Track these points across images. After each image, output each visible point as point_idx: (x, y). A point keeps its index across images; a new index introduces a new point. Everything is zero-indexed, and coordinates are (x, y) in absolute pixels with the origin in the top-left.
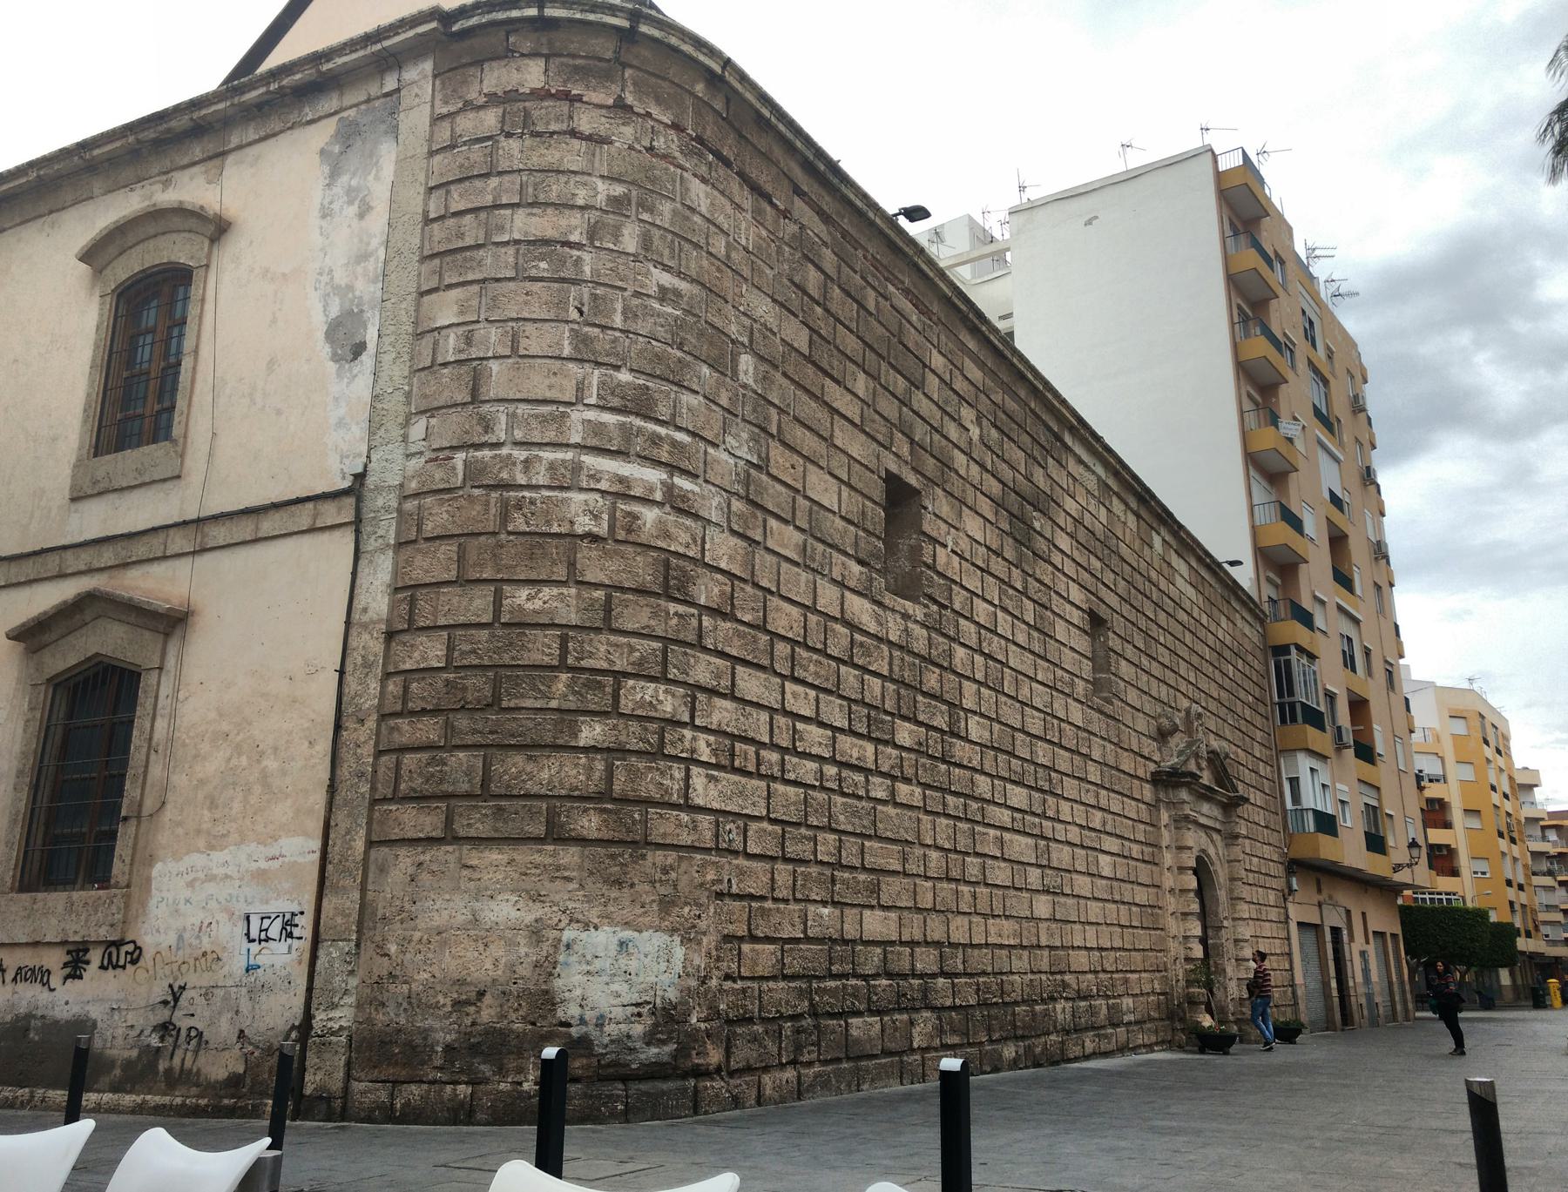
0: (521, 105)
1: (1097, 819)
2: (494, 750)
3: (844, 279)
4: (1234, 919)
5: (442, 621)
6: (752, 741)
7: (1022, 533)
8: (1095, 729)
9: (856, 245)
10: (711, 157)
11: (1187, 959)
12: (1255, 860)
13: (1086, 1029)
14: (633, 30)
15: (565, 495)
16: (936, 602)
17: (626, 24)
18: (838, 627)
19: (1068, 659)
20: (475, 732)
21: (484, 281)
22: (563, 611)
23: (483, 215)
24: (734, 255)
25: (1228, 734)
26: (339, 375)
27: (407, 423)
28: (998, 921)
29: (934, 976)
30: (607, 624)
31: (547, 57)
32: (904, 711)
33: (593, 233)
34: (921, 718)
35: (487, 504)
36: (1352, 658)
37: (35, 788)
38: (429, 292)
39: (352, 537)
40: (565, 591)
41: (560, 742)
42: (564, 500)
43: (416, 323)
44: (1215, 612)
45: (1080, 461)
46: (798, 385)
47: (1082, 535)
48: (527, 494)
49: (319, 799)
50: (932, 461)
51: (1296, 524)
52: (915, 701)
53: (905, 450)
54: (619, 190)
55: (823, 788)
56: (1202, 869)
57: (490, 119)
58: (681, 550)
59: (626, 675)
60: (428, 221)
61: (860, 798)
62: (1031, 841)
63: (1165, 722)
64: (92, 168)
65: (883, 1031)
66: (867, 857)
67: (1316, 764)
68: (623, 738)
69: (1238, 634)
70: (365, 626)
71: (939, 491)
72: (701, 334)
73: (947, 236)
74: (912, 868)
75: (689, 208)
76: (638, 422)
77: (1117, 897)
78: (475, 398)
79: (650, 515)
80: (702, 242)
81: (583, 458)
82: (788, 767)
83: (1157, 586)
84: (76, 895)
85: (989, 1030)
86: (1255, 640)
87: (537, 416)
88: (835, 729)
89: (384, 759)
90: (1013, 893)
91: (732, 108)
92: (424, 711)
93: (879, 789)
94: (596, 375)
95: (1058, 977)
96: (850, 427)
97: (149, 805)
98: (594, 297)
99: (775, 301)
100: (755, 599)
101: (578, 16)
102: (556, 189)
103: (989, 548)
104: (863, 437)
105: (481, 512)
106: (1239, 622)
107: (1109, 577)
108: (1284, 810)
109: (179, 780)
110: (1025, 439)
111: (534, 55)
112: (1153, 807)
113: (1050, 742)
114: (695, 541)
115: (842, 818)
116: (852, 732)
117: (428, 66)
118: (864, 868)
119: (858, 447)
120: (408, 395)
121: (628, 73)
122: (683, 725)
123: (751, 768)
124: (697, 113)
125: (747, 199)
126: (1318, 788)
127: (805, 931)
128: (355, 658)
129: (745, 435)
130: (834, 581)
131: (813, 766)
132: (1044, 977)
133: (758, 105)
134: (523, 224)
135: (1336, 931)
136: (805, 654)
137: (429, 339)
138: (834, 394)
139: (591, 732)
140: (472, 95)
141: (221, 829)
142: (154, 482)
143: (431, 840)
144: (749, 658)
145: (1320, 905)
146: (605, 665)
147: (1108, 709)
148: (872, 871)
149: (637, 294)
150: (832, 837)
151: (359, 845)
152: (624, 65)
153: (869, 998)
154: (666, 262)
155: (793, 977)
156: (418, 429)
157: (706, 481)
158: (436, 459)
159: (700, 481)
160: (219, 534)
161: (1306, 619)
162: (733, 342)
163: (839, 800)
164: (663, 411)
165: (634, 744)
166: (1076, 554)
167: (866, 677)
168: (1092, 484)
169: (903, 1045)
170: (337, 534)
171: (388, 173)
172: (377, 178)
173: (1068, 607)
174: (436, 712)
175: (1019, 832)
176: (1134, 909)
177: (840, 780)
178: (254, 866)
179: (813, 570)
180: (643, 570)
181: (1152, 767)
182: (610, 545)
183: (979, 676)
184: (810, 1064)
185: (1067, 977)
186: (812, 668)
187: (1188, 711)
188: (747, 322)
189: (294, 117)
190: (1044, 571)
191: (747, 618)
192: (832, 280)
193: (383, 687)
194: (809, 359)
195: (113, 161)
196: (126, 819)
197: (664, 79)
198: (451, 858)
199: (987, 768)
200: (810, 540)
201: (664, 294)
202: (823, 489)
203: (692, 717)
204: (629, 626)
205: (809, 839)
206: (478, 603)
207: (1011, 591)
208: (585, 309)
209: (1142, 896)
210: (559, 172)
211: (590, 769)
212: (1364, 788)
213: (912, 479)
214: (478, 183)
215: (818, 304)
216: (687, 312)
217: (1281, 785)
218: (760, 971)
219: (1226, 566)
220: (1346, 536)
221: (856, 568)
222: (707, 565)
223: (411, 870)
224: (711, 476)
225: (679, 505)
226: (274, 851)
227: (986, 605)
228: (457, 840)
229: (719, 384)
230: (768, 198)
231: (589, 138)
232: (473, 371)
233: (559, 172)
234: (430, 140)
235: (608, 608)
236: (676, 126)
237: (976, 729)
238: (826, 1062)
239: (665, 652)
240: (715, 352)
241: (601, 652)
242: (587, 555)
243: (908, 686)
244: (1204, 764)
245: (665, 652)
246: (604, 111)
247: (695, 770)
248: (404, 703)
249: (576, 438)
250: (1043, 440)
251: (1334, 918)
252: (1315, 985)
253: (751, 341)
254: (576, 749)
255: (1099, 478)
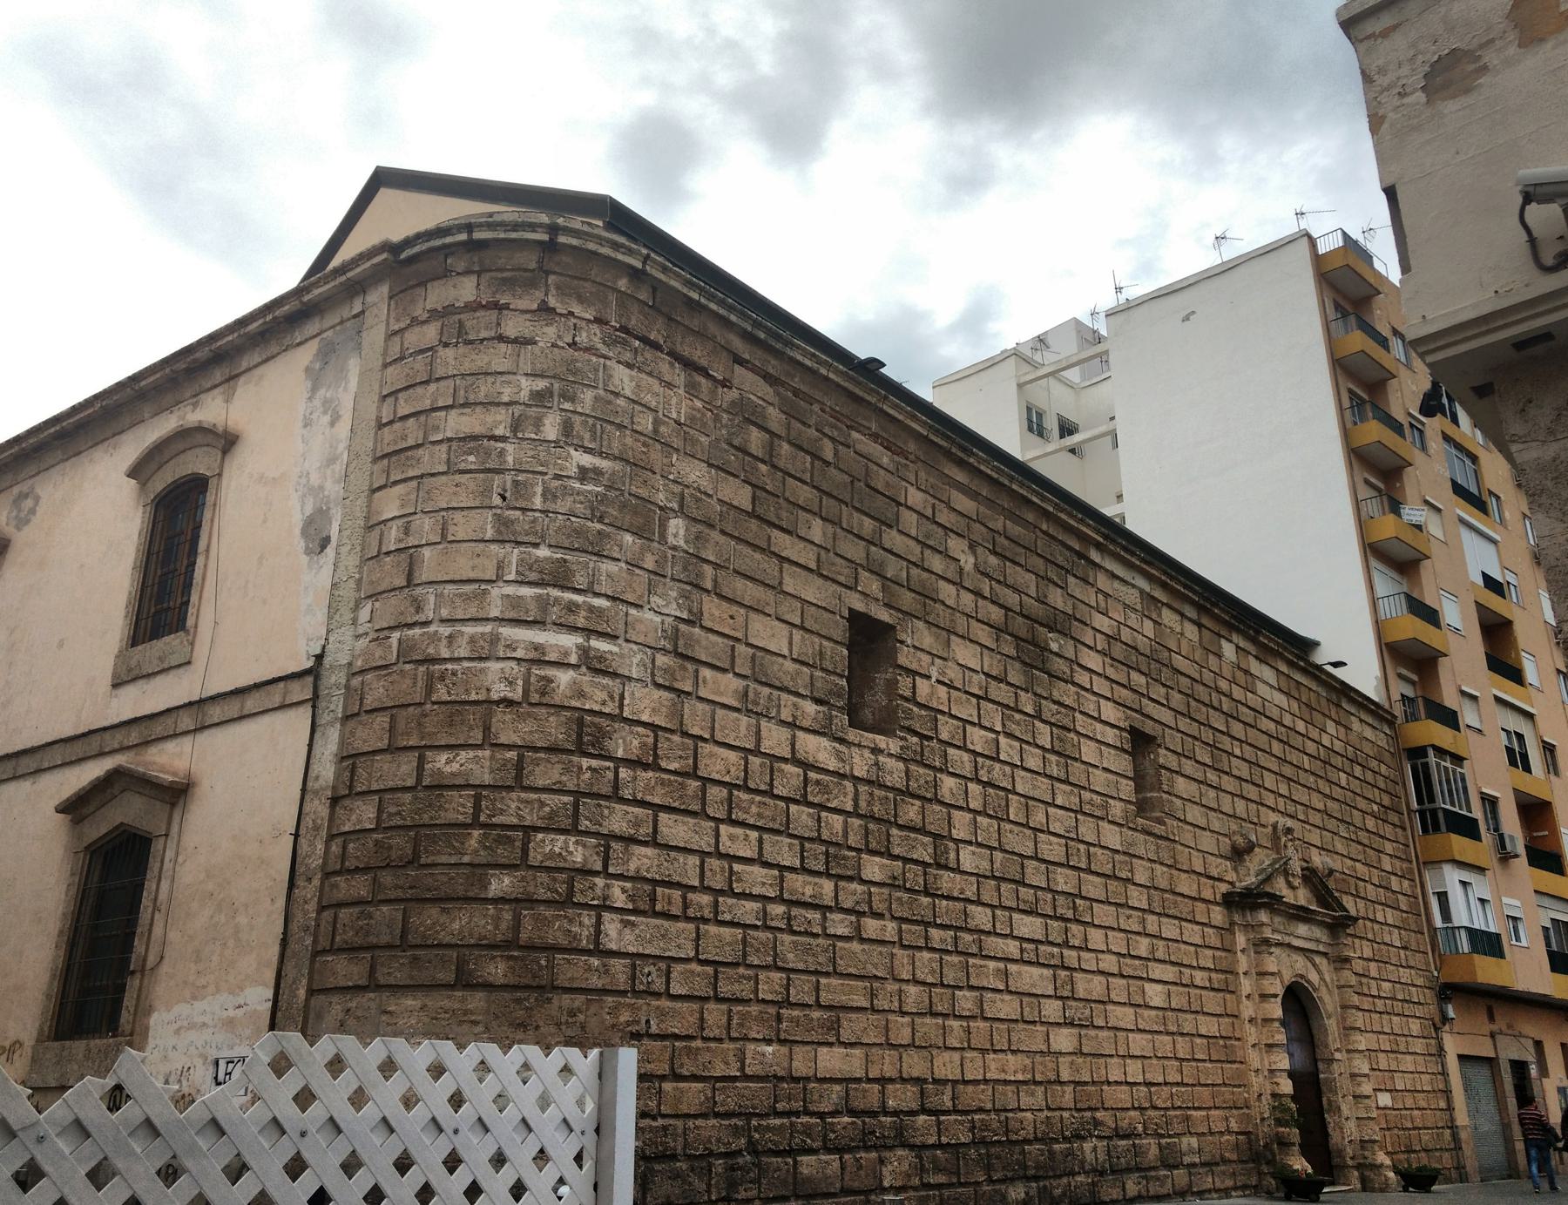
1: (1142, 946)
2: (412, 904)
3: (793, 434)
4: (1349, 1051)
5: (375, 787)
6: (678, 885)
7: (1033, 657)
8: (1141, 851)
9: (811, 400)
10: (637, 343)
11: (1274, 1095)
12: (1386, 985)
13: (1129, 1170)
16: (916, 733)
17: (546, 237)
19: (1099, 780)
20: (397, 887)
21: (422, 476)
23: (422, 418)
24: (663, 429)
25: (1339, 847)
26: (310, 567)
27: (356, 608)
28: (1001, 1056)
29: (912, 1113)
30: (519, 784)
31: (479, 273)
32: (873, 845)
33: (516, 426)
34: (896, 851)
35: (415, 678)
36: (1524, 757)
38: (380, 488)
39: (310, 710)
40: (480, 753)
41: (471, 894)
42: (482, 670)
43: (367, 518)
44: (1318, 717)
45: (1114, 576)
46: (739, 540)
47: (1118, 650)
48: (449, 666)
50: (910, 595)
51: (1431, 616)
52: (889, 835)
54: (541, 384)
56: (1298, 1001)
57: (430, 333)
58: (596, 708)
59: (536, 829)
60: (381, 426)
61: (816, 936)
62: (1047, 972)
63: (1240, 840)
64: (142, 396)
65: (843, 1169)
66: (823, 994)
67: (1466, 876)
68: (531, 889)
69: (1353, 738)
70: (316, 793)
71: (920, 624)
72: (623, 506)
73: (1050, 341)
75: (612, 392)
77: (1173, 1029)
78: (410, 583)
79: (564, 678)
80: (626, 422)
81: (501, 630)
82: (721, 908)
83: (1230, 696)
85: (988, 1168)
86: (1383, 744)
87: (460, 595)
88: (782, 868)
89: (325, 914)
90: (1021, 1026)
91: (659, 295)
93: (840, 925)
95: (1088, 1114)
96: (804, 573)
97: (152, 959)
98: (516, 483)
99: (710, 465)
100: (684, 747)
101: (502, 235)
102: (484, 389)
103: (987, 675)
104: (820, 581)
105: (408, 685)
106: (1356, 726)
107: (1158, 692)
108: (1433, 931)
109: (173, 935)
110: (1039, 563)
111: (468, 272)
112: (1230, 929)
113: (1073, 868)
114: (612, 697)
115: (790, 956)
117: (384, 289)
118: (819, 1006)
119: (813, 590)
120: (359, 582)
121: (551, 279)
123: (676, 911)
125: (678, 376)
126: (1475, 905)
128: (308, 821)
129: (674, 594)
130: (783, 723)
131: (756, 906)
132: (1066, 1114)
133: (685, 290)
134: (457, 423)
135: (1519, 1067)
136: (744, 796)
137: (377, 531)
139: (502, 884)
140: (418, 312)
141: (202, 981)
142: (171, 668)
143: (358, 989)
144: (676, 805)
145: (1492, 1035)
146: (515, 821)
147: (1159, 829)
148: (830, 1008)
149: (557, 477)
150: (777, 976)
151: (302, 993)
152: (548, 273)
153: (825, 1136)
154: (587, 444)
156: (364, 614)
157: (627, 641)
158: (377, 639)
159: (620, 641)
161: (1450, 719)
162: (661, 508)
163: (787, 938)
164: (580, 580)
165: (542, 894)
166: (1110, 672)
167: (824, 814)
168: (1132, 597)
169: (869, 1183)
172: (345, 389)
173: (1099, 726)
174: (366, 870)
175: (1030, 963)
176: (1198, 1041)
177: (789, 919)
178: (225, 1014)
180: (555, 729)
181: (1224, 888)
182: (525, 708)
183: (975, 804)
185: (1098, 1115)
186: (754, 809)
187: (1275, 827)
188: (677, 489)
189: (287, 341)
190: (1066, 694)
191: (673, 766)
192: (780, 437)
194: (752, 514)
196: (133, 973)
197: (585, 280)
198: (373, 1005)
199: (986, 898)
200: (753, 685)
201: (584, 474)
202: (770, 635)
203: (605, 866)
204: (540, 783)
205: (749, 978)
206: (405, 768)
207: (1017, 716)
208: (508, 495)
209: (1208, 1026)
210: (487, 374)
211: (497, 919)
212: (1547, 902)
213: (884, 615)
214: (419, 390)
215: (763, 461)
217: (1426, 904)
218: (684, 1109)
219: (1329, 669)
220: (1510, 623)
221: (810, 708)
222: (626, 720)
224: (632, 636)
225: (595, 665)
228: (380, 987)
229: (643, 550)
230: (704, 372)
231: (515, 341)
232: (409, 555)
233: (487, 374)
234: (385, 354)
235: (519, 766)
236: (599, 321)
237: (969, 859)
239: (576, 805)
241: (513, 808)
242: (501, 716)
243: (879, 820)
244: (1297, 882)
245: (576, 805)
246: (528, 316)
247: (607, 916)
248: (343, 862)
250: (1060, 560)
251: (1510, 1051)
252: (1489, 1125)
253: (681, 506)
255: (1142, 591)
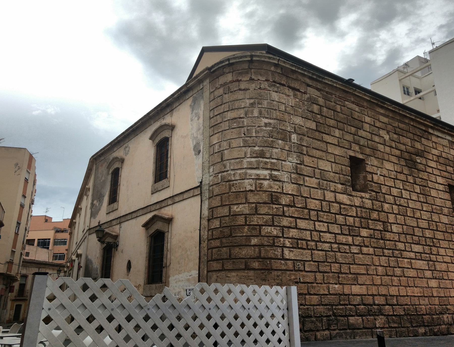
0: (227, 86)
5: (219, 216)
6: (305, 240)
7: (411, 164)
9: (331, 94)
14: (252, 60)
15: (243, 181)
17: (250, 59)
18: (335, 204)
20: (227, 243)
21: (222, 131)
22: (245, 210)
23: (221, 115)
24: (287, 109)
27: (209, 168)
28: (412, 288)
30: (256, 213)
31: (232, 72)
32: (363, 226)
37: (149, 260)
38: (212, 136)
40: (245, 205)
42: (244, 182)
45: (438, 137)
46: (313, 138)
48: (235, 182)
49: (197, 261)
50: (368, 149)
52: (368, 222)
53: (357, 148)
54: (252, 101)
55: (332, 251)
57: (221, 91)
58: (276, 191)
59: (263, 225)
61: (348, 253)
68: (263, 242)
70: (204, 218)
71: (373, 158)
74: (370, 272)
75: (272, 100)
76: (261, 159)
78: (222, 160)
79: (266, 183)
81: (247, 171)
84: (157, 285)
85: (411, 323)
88: (335, 234)
89: (209, 250)
90: (418, 279)
92: (216, 238)
93: (355, 250)
94: (249, 149)
97: (168, 264)
98: (248, 130)
99: (302, 117)
100: (302, 200)
101: (238, 60)
102: (237, 104)
103: (396, 172)
104: (339, 148)
105: (224, 188)
109: (172, 257)
114: (280, 187)
115: (340, 259)
116: (342, 234)
117: (208, 81)
118: (350, 273)
119: (338, 151)
120: (209, 161)
121: (252, 70)
122: (281, 237)
124: (273, 75)
125: (291, 93)
127: (329, 292)
128: (202, 226)
129: (295, 156)
130: (332, 191)
132: (436, 307)
133: (291, 67)
134: (230, 115)
136: (322, 213)
137: (212, 147)
138: (327, 138)
139: (254, 241)
140: (217, 86)
143: (219, 271)
144: (302, 217)
146: (256, 223)
148: (354, 274)
149: (259, 127)
150: (337, 265)
151: (205, 272)
152: (251, 69)
154: (266, 116)
155: (326, 305)
156: (211, 170)
157: (282, 171)
159: (281, 171)
160: (177, 199)
162: (289, 132)
163: (339, 254)
164: (268, 155)
165: (266, 243)
167: (347, 217)
170: (196, 198)
171: (202, 108)
174: (218, 238)
179: (323, 189)
180: (265, 197)
182: (256, 192)
184: (334, 330)
186: (325, 217)
188: (293, 126)
189: (184, 99)
191: (300, 206)
192: (323, 106)
193: (208, 233)
194: (317, 130)
195: (154, 116)
197: (262, 69)
198: (224, 275)
200: (321, 181)
202: (325, 165)
203: (283, 235)
204: (262, 213)
211: (255, 251)
213: (361, 156)
214: (219, 107)
215: (318, 114)
216: (274, 128)
218: (313, 303)
221: (340, 186)
222: (284, 194)
223: (216, 278)
224: (284, 169)
225: (274, 179)
226: (190, 274)
227: (396, 190)
228: (225, 270)
229: (285, 145)
230: (298, 90)
231: (244, 90)
232: (221, 153)
234: (210, 98)
235: (256, 208)
236: (267, 80)
238: (340, 330)
239: (273, 218)
240: (283, 136)
241: (255, 220)
242: (250, 195)
245: (273, 218)
246: (247, 82)
247: (285, 249)
249: (245, 166)
250: (418, 134)
253: (295, 130)
254: (251, 245)
255: (449, 140)
